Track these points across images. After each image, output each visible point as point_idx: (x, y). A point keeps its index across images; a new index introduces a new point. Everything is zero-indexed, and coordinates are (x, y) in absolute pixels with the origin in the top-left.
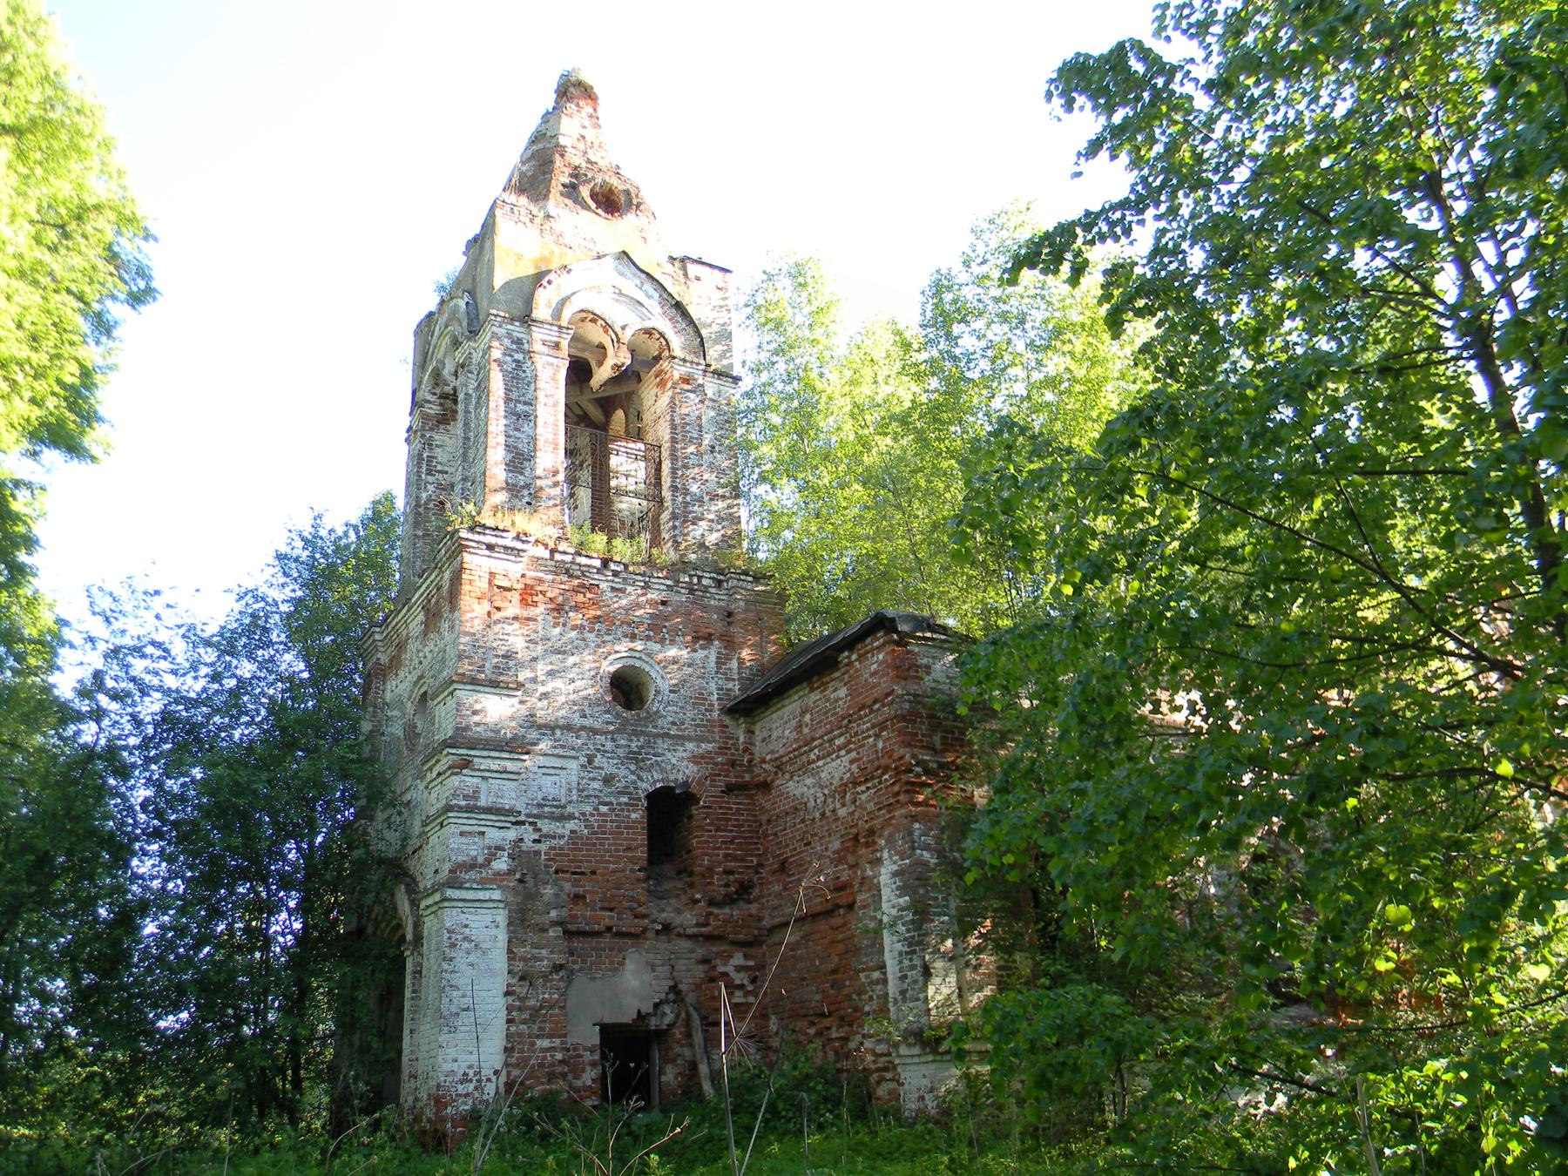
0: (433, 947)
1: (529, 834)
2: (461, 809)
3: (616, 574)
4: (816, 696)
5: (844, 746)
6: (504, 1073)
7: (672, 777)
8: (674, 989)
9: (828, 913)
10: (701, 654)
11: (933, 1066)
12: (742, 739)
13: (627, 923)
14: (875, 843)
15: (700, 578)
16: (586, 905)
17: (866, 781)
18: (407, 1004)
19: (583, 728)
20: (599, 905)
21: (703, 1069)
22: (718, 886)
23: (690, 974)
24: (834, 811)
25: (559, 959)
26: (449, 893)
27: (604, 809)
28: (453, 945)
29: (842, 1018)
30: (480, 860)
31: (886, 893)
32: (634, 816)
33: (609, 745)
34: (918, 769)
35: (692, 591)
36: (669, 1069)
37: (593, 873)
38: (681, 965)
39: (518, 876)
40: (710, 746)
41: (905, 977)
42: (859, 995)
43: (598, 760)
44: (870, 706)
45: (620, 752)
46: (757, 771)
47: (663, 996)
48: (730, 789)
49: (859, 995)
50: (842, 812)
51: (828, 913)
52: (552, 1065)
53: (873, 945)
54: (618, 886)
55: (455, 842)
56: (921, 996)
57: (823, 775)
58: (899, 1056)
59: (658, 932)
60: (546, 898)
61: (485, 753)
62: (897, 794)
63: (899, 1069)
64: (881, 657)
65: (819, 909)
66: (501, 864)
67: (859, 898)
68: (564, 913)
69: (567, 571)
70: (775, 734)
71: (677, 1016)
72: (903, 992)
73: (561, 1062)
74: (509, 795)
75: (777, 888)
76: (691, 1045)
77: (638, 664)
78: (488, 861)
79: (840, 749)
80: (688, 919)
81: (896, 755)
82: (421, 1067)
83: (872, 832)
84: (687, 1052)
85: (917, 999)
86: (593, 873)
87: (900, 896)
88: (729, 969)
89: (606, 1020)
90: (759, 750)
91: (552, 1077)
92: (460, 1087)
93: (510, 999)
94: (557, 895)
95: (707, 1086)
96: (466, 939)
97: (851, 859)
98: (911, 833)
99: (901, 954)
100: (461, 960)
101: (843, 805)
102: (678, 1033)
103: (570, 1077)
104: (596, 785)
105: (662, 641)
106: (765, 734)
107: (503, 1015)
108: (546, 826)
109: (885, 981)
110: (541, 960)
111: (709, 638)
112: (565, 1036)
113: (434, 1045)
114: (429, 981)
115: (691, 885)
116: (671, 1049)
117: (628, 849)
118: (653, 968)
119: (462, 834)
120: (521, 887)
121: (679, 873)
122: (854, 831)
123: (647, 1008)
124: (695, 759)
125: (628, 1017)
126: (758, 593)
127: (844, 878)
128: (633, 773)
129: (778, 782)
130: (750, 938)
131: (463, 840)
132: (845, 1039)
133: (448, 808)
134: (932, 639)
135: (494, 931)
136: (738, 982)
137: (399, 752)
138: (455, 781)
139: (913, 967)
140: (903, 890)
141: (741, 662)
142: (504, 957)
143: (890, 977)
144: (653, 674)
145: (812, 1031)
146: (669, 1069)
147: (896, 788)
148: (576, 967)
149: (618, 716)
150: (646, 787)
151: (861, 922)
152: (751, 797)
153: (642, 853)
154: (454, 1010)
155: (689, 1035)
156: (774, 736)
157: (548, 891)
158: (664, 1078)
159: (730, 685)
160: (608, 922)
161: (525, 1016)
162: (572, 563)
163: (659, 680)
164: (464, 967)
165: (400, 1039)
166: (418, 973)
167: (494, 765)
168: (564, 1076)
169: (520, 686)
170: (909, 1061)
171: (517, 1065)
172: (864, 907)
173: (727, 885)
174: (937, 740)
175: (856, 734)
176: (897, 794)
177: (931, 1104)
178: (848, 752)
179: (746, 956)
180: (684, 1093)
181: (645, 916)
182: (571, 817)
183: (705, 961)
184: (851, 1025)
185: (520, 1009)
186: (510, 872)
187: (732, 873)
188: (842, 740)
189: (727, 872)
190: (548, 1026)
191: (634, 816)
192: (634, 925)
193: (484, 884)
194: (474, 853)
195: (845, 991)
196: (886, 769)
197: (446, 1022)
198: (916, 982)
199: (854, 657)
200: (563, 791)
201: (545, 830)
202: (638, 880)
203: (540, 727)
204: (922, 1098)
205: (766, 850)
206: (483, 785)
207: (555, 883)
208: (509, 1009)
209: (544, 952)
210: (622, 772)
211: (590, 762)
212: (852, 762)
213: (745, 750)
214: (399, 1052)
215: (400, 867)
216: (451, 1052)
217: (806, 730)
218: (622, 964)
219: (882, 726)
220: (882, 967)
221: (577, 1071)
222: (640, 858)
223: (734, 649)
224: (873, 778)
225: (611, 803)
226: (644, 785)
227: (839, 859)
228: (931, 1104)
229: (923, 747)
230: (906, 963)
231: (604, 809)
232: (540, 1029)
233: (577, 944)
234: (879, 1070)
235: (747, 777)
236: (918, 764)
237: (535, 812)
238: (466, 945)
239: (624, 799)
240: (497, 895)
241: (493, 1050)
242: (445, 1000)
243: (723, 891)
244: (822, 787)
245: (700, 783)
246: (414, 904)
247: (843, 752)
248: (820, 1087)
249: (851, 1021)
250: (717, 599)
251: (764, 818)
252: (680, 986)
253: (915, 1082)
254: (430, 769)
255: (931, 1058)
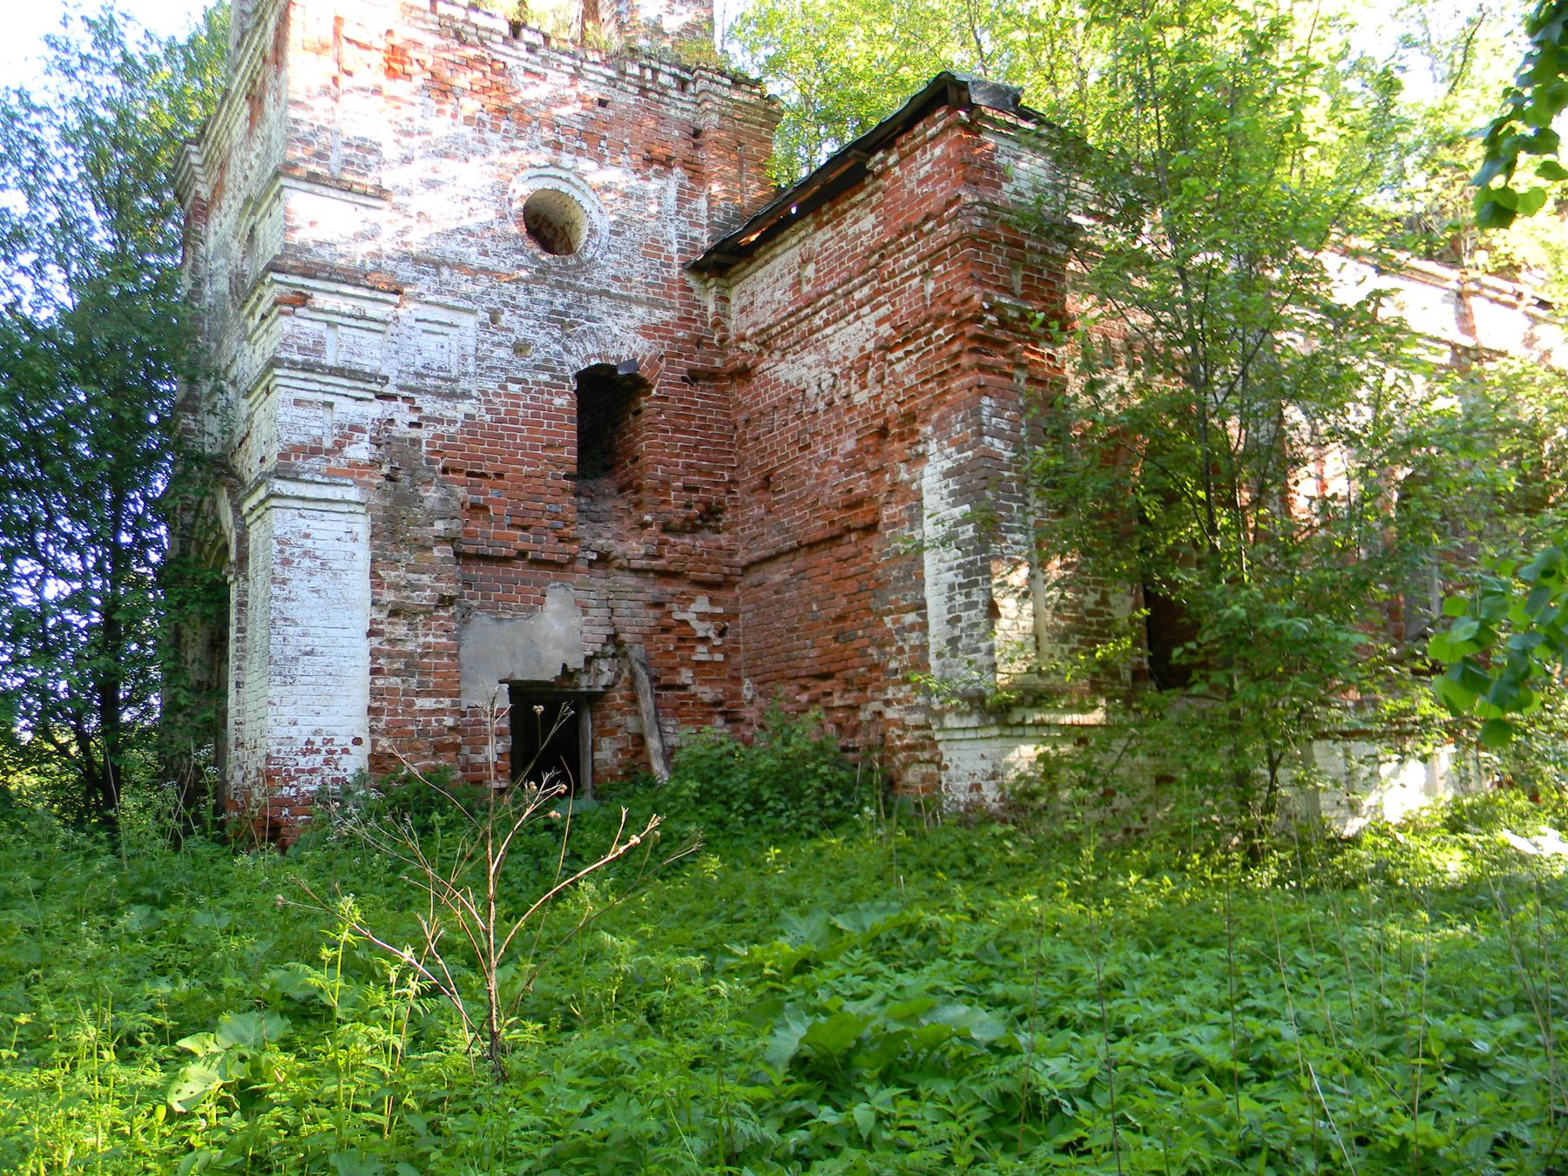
0: (260, 565)
1: (402, 415)
2: (293, 365)
3: (532, 49)
4: (826, 233)
5: (870, 299)
6: (367, 741)
7: (613, 353)
8: (613, 638)
9: (833, 540)
10: (654, 185)
11: (998, 743)
12: (711, 308)
13: (548, 548)
14: (915, 432)
15: (655, 71)
16: (489, 519)
17: (906, 341)
18: (232, 648)
19: (484, 270)
20: (508, 521)
21: (653, 743)
22: (675, 507)
23: (635, 620)
24: (847, 397)
25: (447, 588)
26: (279, 486)
27: (514, 388)
28: (286, 562)
29: (848, 681)
30: (328, 443)
31: (930, 501)
32: (558, 401)
33: (522, 299)
34: (992, 318)
35: (643, 91)
36: (606, 743)
37: (500, 476)
38: (624, 608)
39: (385, 470)
40: (667, 316)
41: (958, 619)
42: (881, 646)
43: (506, 318)
44: (916, 227)
45: (539, 310)
46: (731, 353)
47: (598, 647)
48: (693, 377)
49: (881, 646)
50: (860, 398)
51: (833, 540)
52: (439, 733)
53: (908, 576)
54: (536, 496)
55: (287, 414)
56: (983, 645)
57: (832, 347)
58: (942, 729)
59: (591, 563)
60: (428, 504)
61: (332, 287)
62: (957, 355)
63: (941, 747)
64: (937, 152)
65: (820, 535)
66: (360, 451)
67: (886, 513)
68: (455, 525)
69: (458, 35)
70: (760, 299)
71: (618, 676)
72: (952, 642)
73: (451, 729)
74: (371, 353)
75: (757, 511)
76: (637, 713)
77: (564, 188)
78: (339, 446)
79: (861, 305)
80: (634, 548)
81: (956, 299)
82: (248, 734)
83: (911, 417)
84: (630, 722)
85: (977, 650)
86: (500, 476)
87: (955, 505)
88: (689, 616)
89: (518, 677)
90: (736, 324)
91: (439, 749)
92: (302, 761)
93: (375, 641)
94: (444, 501)
95: (658, 766)
96: (306, 553)
97: (872, 463)
98: (977, 412)
99: (951, 587)
100: (298, 582)
101: (863, 387)
102: (618, 697)
103: (466, 750)
104: (503, 353)
105: (600, 158)
106: (745, 301)
107: (365, 663)
108: (429, 406)
109: (924, 627)
110: (421, 588)
111: (667, 163)
112: (458, 694)
113: (263, 701)
114: (256, 613)
115: (638, 505)
116: (608, 717)
117: (550, 446)
118: (585, 610)
119: (297, 402)
120: (390, 485)
121: (621, 490)
122: (879, 422)
123: (576, 662)
124: (647, 331)
125: (550, 672)
126: (738, 106)
127: (861, 489)
128: (557, 341)
129: (764, 366)
130: (718, 578)
131: (299, 411)
132: (854, 708)
133: (274, 363)
134: (1015, 127)
135: (350, 546)
136: (700, 634)
137: (225, 313)
138: (284, 325)
139: (971, 606)
140: (959, 497)
141: (711, 199)
142: (366, 582)
143: (932, 621)
144: (587, 207)
145: (804, 698)
146: (606, 743)
147: (955, 348)
148: (475, 603)
149: (534, 259)
150: (576, 362)
151: (895, 540)
152: (722, 390)
153: (569, 454)
154: (290, 652)
155: (634, 700)
156: (758, 303)
157: (432, 495)
158: (598, 755)
159: (696, 233)
160: (520, 545)
161: (399, 665)
162: (466, 22)
163: (595, 215)
164: (305, 594)
165: (225, 694)
166: (242, 604)
167: (346, 306)
168: (456, 748)
169: (381, 193)
170: (959, 735)
171: (386, 733)
172: (895, 525)
173: (688, 506)
174: (1017, 281)
175: (892, 274)
176: (957, 355)
177: (990, 793)
178: (873, 309)
179: (712, 601)
180: (626, 774)
181: (573, 540)
182: (465, 395)
183: (658, 605)
184: (863, 689)
185: (389, 655)
186: (374, 464)
187: (696, 490)
188: (866, 290)
189: (689, 489)
190: (432, 680)
191: (558, 401)
192: (561, 552)
193: (333, 477)
194: (318, 432)
195: (856, 644)
196: (940, 320)
197: (283, 671)
198: (976, 625)
199: (892, 160)
200: (454, 358)
201: (427, 411)
202: (564, 490)
203: (417, 260)
204: (978, 787)
205: (742, 461)
206: (330, 335)
207: (442, 485)
208: (375, 654)
209: (426, 579)
210: (541, 338)
211: (494, 320)
212: (879, 323)
213: (716, 325)
214: (223, 714)
215: (225, 466)
216: (288, 712)
217: (806, 288)
218: (540, 602)
219: (935, 257)
220: (920, 607)
221: (478, 744)
222: (567, 461)
223: (702, 183)
224: (917, 336)
225: (525, 381)
226: (573, 360)
227: (854, 463)
228: (990, 793)
229: (996, 287)
230: (960, 599)
231: (514, 388)
232: (420, 683)
233: (476, 571)
234: (909, 748)
235: (718, 362)
236: (991, 311)
237: (412, 383)
238: (307, 562)
239: (544, 377)
240: (353, 494)
241: (351, 711)
242: (276, 639)
243: (682, 513)
244: (830, 365)
245: (651, 364)
246: (237, 508)
247: (866, 309)
248: (824, 769)
249: (870, 679)
250: (679, 108)
251: (741, 418)
252: (623, 636)
253: (968, 766)
254: (252, 313)
255: (995, 731)
